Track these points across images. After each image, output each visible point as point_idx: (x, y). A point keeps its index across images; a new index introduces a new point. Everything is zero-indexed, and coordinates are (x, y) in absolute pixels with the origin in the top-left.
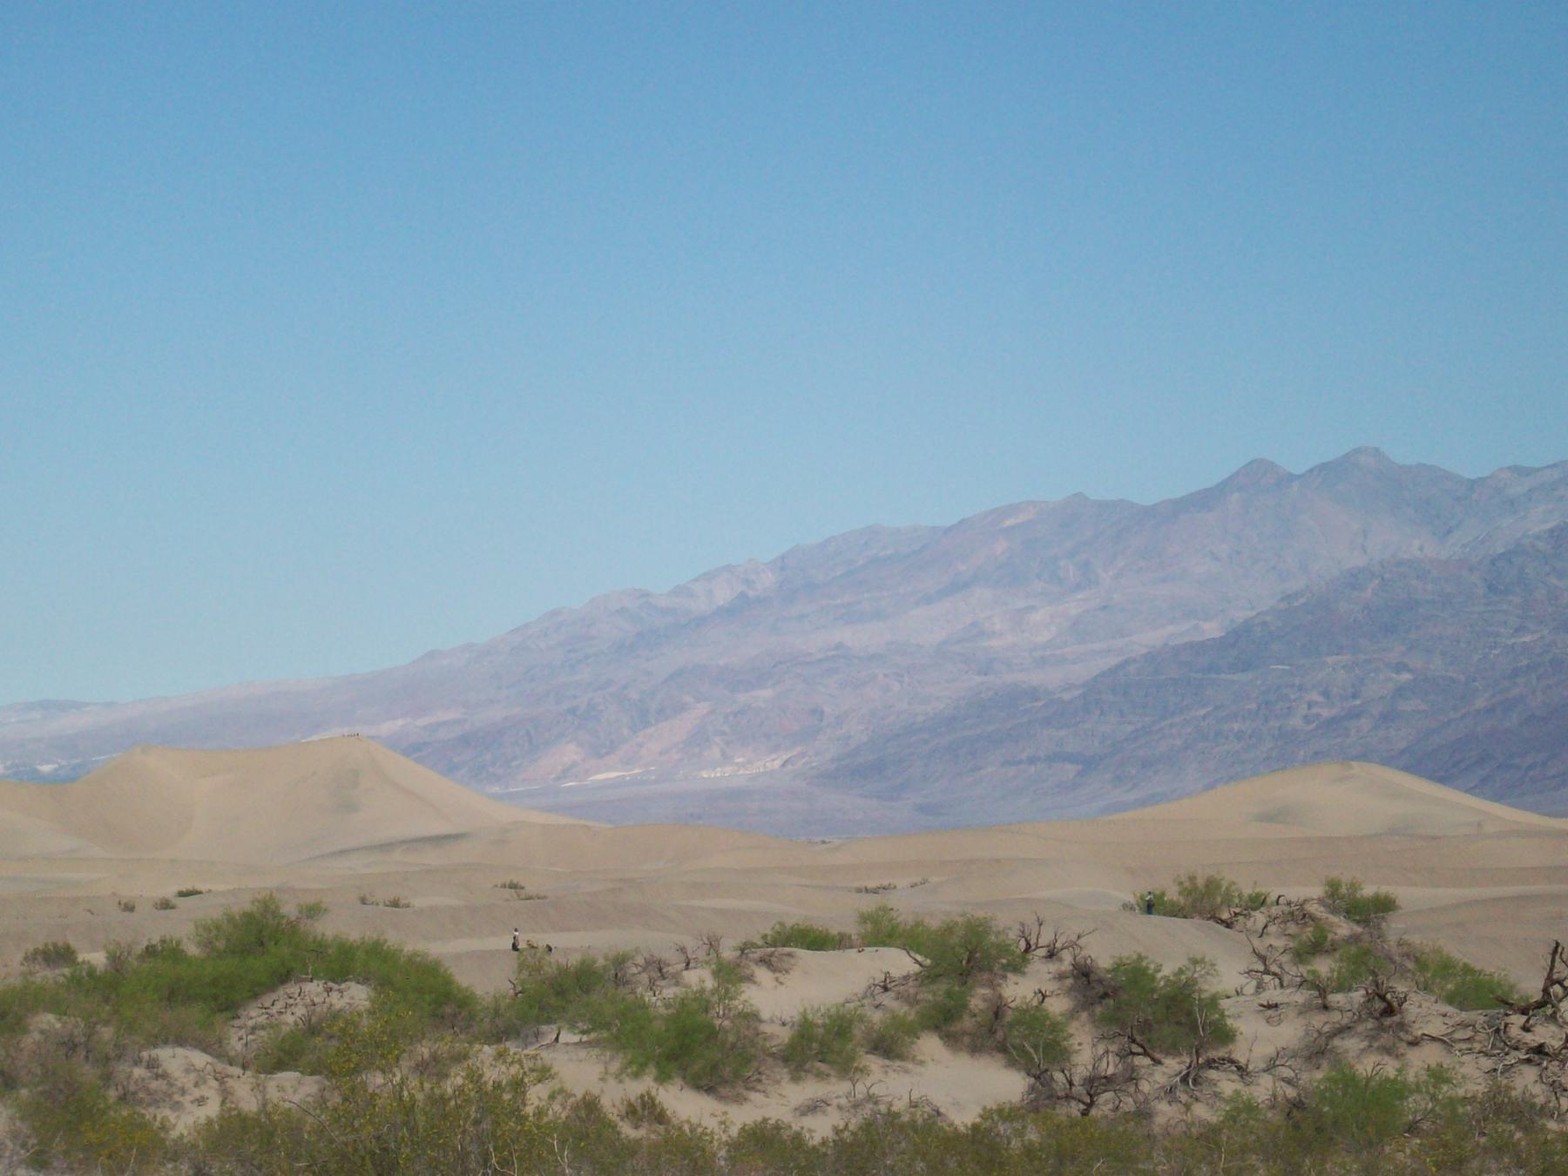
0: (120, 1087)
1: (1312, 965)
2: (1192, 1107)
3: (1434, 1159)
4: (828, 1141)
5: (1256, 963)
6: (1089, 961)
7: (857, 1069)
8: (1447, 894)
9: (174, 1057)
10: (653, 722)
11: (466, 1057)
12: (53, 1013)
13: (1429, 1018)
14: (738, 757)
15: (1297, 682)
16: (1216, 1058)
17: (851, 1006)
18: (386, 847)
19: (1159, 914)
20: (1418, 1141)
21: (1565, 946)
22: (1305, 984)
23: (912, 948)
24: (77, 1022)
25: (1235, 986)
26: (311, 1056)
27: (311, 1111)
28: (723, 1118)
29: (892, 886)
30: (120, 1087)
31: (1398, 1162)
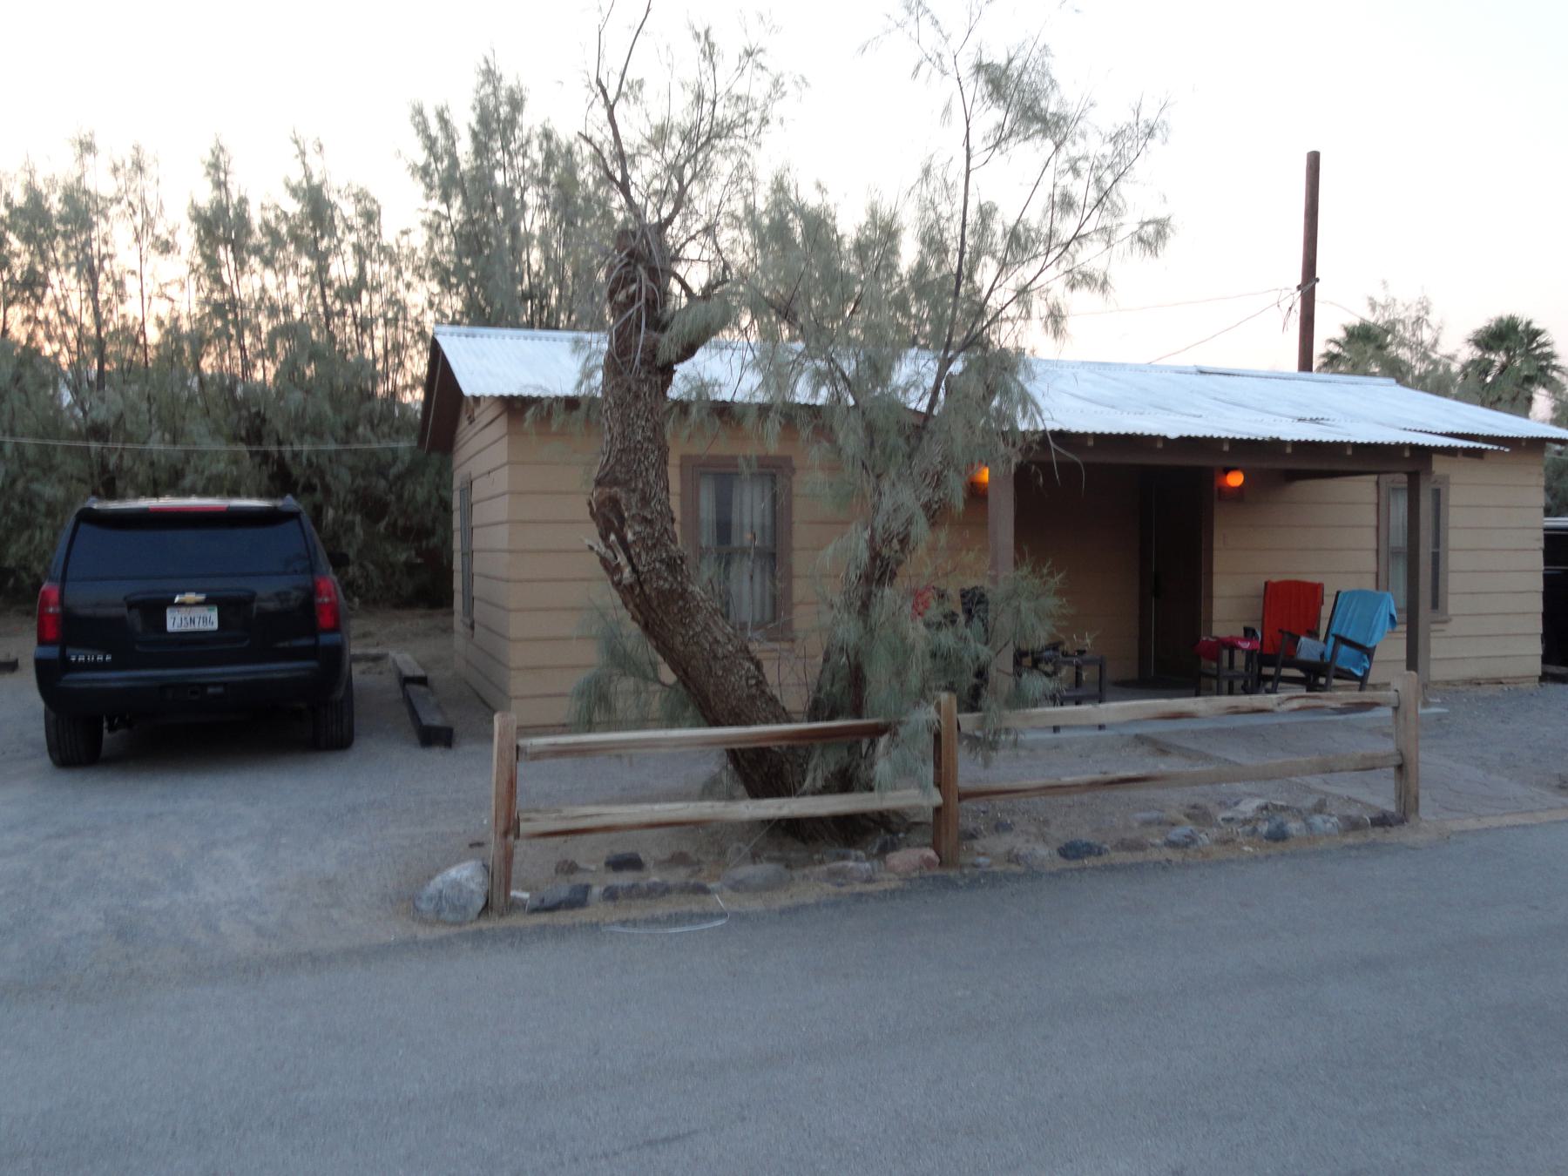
0: (380, 434)
1: (922, 856)
2: (481, 79)
3: (253, 306)
4: (243, 222)
5: (1008, 674)
6: (736, 778)
7: (690, 382)
8: (675, 504)
9: (262, 208)
10: (355, 389)
11: (1426, 349)
12: (1234, 488)
13: (739, 71)
14: (1248, 852)
15: (748, 771)
16: (554, 137)
17: (747, 871)
18: (1357, 384)
19: (861, 791)
20: (35, 564)
21: (360, 182)
22: (131, 211)
23: (792, 748)
24: (343, 233)
25: (1550, 330)
26: (638, 550)
27: (1260, 816)
28: (1039, 307)
29: (418, 119)
30: (380, 434)
31: (901, 835)
